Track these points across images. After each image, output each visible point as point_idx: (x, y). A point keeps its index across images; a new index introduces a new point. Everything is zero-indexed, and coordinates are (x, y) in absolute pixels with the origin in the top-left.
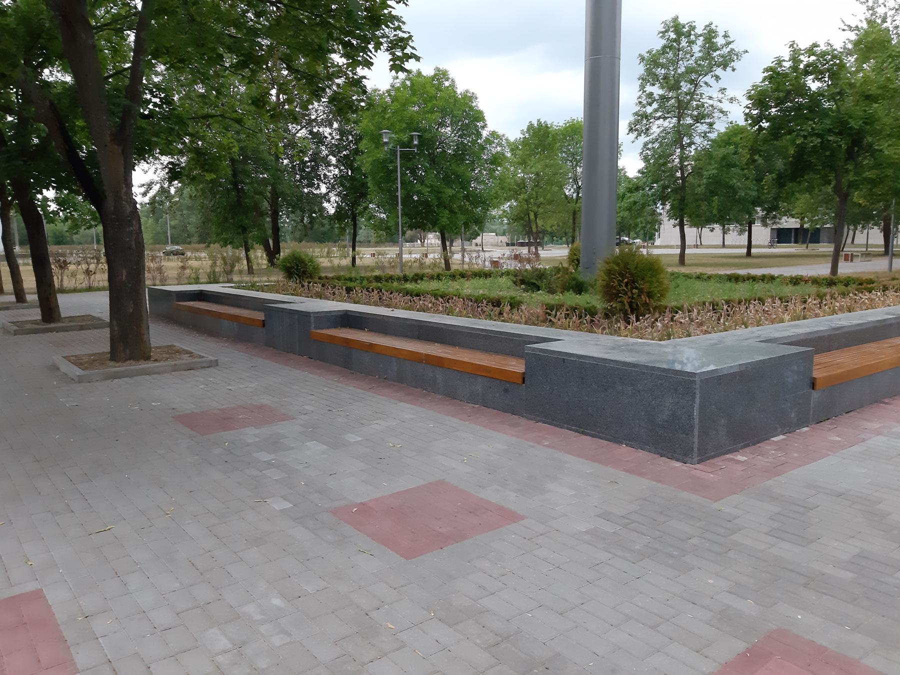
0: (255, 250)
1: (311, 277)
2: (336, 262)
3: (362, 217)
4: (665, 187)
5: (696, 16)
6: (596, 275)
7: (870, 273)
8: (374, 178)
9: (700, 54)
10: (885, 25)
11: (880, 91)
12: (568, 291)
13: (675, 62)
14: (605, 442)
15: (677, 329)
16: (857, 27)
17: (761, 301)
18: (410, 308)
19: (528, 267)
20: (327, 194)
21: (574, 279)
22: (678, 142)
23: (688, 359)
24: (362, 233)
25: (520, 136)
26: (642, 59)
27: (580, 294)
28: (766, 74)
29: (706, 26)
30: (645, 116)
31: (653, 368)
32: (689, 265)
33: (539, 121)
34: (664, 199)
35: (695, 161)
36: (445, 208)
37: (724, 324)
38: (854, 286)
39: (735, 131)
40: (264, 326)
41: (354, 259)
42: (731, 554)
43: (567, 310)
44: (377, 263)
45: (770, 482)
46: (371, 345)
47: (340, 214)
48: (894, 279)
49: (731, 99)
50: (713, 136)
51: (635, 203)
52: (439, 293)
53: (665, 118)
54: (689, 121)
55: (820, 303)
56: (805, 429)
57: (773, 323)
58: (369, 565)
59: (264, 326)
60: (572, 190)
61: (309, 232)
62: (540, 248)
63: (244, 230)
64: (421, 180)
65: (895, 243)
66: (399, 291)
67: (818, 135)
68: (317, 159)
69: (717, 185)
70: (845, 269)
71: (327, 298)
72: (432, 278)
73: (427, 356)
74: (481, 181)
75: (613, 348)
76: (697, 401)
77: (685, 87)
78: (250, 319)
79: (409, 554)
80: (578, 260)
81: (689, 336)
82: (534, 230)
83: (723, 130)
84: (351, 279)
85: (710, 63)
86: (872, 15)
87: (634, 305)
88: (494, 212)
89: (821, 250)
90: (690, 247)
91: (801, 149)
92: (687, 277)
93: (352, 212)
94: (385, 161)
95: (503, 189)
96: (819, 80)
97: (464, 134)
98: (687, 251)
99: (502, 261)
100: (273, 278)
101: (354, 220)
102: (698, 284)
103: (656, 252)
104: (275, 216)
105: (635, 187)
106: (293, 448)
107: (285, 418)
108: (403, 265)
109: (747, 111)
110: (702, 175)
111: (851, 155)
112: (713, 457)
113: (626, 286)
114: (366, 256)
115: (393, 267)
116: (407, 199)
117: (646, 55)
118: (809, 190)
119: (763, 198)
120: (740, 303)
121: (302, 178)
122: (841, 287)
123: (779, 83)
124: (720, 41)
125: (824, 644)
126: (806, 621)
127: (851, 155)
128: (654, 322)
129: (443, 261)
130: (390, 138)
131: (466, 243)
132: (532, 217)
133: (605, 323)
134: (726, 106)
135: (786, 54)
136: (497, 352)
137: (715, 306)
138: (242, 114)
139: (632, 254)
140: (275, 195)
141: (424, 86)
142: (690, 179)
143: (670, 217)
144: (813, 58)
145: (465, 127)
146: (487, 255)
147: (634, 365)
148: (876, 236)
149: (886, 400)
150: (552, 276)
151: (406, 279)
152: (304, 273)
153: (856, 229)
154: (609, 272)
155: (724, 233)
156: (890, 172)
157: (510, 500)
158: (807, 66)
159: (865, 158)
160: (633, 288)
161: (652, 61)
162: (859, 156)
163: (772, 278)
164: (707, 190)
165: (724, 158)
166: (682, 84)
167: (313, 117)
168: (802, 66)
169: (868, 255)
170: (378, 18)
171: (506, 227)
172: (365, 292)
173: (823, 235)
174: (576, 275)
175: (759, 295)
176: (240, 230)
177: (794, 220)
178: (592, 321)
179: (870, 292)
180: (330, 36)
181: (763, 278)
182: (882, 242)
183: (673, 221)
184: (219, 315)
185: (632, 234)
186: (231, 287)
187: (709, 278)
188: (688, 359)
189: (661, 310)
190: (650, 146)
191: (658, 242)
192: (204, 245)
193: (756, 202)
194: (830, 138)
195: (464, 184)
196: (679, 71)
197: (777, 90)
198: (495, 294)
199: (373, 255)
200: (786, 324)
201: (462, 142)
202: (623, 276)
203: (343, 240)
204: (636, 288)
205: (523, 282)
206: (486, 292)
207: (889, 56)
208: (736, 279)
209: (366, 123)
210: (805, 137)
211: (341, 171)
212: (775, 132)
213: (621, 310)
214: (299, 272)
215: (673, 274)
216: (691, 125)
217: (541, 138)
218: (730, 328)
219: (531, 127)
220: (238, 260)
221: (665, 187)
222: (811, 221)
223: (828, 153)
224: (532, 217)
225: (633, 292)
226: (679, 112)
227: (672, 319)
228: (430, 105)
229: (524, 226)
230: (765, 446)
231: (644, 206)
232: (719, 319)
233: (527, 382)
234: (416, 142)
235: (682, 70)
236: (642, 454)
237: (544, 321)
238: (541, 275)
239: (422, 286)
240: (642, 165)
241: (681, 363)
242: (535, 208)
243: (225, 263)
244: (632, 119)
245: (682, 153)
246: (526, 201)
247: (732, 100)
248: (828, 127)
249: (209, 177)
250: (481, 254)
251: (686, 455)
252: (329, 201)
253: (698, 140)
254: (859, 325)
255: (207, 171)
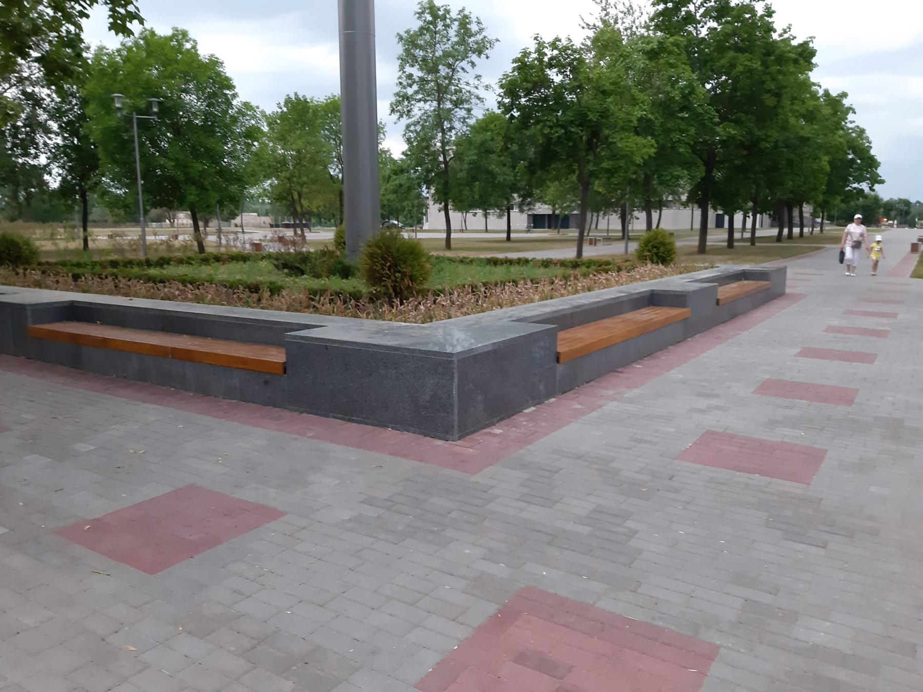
1: (28, 263)
2: (62, 245)
4: (428, 171)
6: (359, 260)
9: (456, 39)
10: (617, 26)
11: (612, 87)
12: (334, 275)
13: (432, 45)
14: (371, 427)
15: (438, 312)
17: (515, 283)
18: (153, 297)
20: (48, 165)
21: (340, 263)
22: (439, 125)
23: (458, 340)
24: (96, 212)
26: (401, 38)
27: (347, 278)
28: (515, 65)
29: (461, 11)
30: (406, 97)
32: (456, 249)
33: (296, 94)
35: (457, 146)
38: (594, 267)
39: (491, 119)
43: (332, 295)
44: (114, 245)
45: (522, 451)
46: (105, 341)
47: (66, 189)
48: (627, 261)
49: (487, 86)
50: (472, 122)
52: (188, 279)
53: (426, 101)
54: (448, 105)
55: (566, 284)
56: (553, 400)
57: (524, 303)
60: (337, 170)
62: (305, 230)
65: (630, 228)
66: (139, 278)
68: (33, 124)
69: (477, 172)
70: (589, 252)
71: (48, 287)
72: (180, 262)
75: (377, 333)
76: (456, 380)
77: (443, 71)
79: (152, 568)
81: (450, 317)
82: (299, 209)
83: (481, 117)
84: (79, 265)
85: (465, 49)
87: (398, 289)
89: (570, 234)
90: (456, 231)
92: (451, 260)
95: (261, 165)
96: (562, 73)
98: (453, 235)
99: (263, 244)
101: (83, 196)
102: (461, 268)
103: (420, 235)
105: (399, 170)
108: (146, 247)
109: (500, 99)
110: (463, 161)
111: (591, 147)
112: (473, 432)
113: (389, 270)
114: (101, 237)
115: (135, 250)
117: (405, 35)
118: (557, 178)
120: (496, 285)
121: (15, 145)
122: (584, 269)
123: (526, 74)
124: (474, 27)
126: (552, 577)
128: (417, 306)
129: (195, 244)
130: (124, 104)
132: (296, 197)
133: (370, 307)
134: (481, 93)
135: (532, 47)
136: (255, 342)
137: (474, 288)
139: (394, 238)
143: (435, 202)
144: (556, 52)
146: (247, 237)
147: (396, 349)
149: (620, 370)
150: (316, 259)
151: (149, 263)
153: (598, 216)
154: (372, 256)
156: (622, 163)
157: (271, 497)
158: (551, 59)
159: (602, 149)
160: (396, 271)
161: (411, 42)
162: (597, 147)
163: (527, 261)
164: (472, 174)
165: (482, 144)
168: (546, 59)
169: (608, 239)
171: (268, 207)
172: (97, 279)
173: (572, 221)
175: (513, 277)
177: (546, 206)
178: (357, 306)
179: (607, 273)
181: (519, 261)
182: (620, 227)
183: (438, 206)
187: (472, 261)
189: (424, 293)
190: (412, 128)
191: (426, 226)
193: (514, 188)
194: (573, 130)
195: (214, 157)
196: (437, 54)
203: (72, 220)
204: (399, 272)
205: (285, 266)
206: (244, 277)
207: (621, 56)
208: (495, 262)
210: (551, 128)
211: (65, 138)
213: (385, 294)
215: (437, 258)
216: (450, 110)
217: (299, 113)
219: (288, 101)
222: (561, 207)
223: (571, 144)
224: (296, 197)
225: (396, 276)
227: (435, 302)
228: (169, 69)
230: (518, 418)
231: (410, 189)
232: (477, 301)
233: (289, 371)
234: (155, 110)
235: (439, 53)
236: (407, 436)
237: (308, 307)
240: (405, 147)
244: (393, 99)
245: (443, 137)
246: (289, 179)
250: (240, 236)
251: (447, 433)
252: (50, 174)
253: (457, 125)
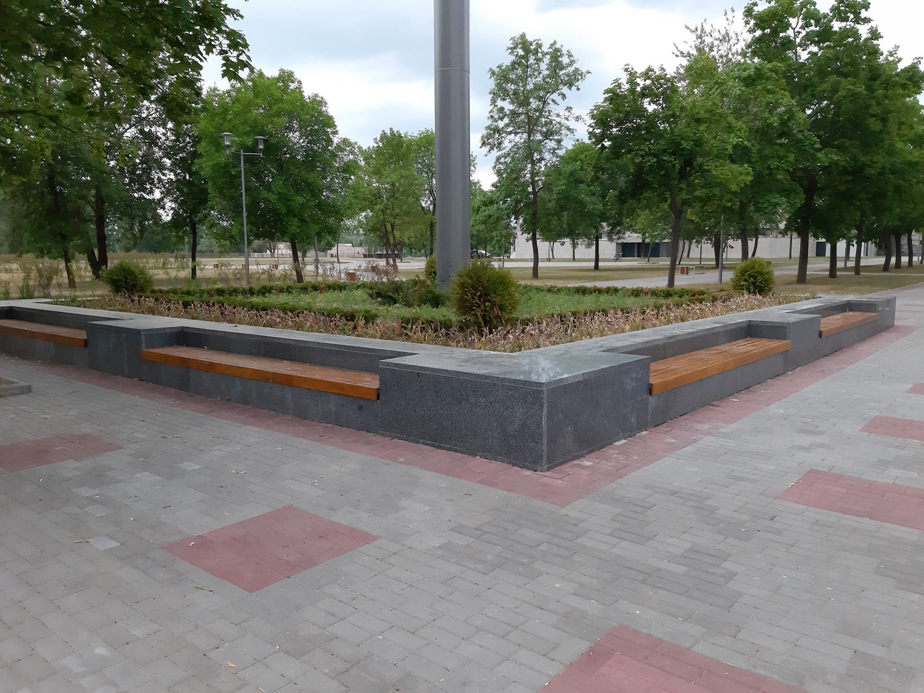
0: (78, 262)
1: (142, 291)
2: (173, 273)
3: (203, 225)
5: (543, 32)
6: (450, 290)
7: (704, 285)
8: (215, 184)
9: (547, 72)
10: (713, 53)
11: (707, 115)
12: (425, 303)
13: (524, 79)
15: (527, 340)
16: (689, 53)
17: (605, 312)
18: (256, 324)
19: (385, 280)
20: (162, 199)
21: (431, 292)
22: (529, 157)
24: (204, 242)
25: (372, 144)
26: (493, 73)
27: (437, 307)
28: (607, 96)
30: (497, 130)
31: (503, 380)
32: (542, 278)
33: (391, 129)
34: (517, 214)
35: (546, 176)
36: (294, 216)
37: (571, 335)
38: (687, 297)
39: (581, 149)
40: (86, 346)
41: (194, 270)
42: (576, 557)
43: (423, 323)
44: (220, 274)
45: (612, 485)
46: (212, 365)
47: (176, 222)
48: (722, 290)
49: (577, 117)
50: (561, 152)
51: (490, 216)
53: (516, 134)
54: (539, 137)
56: (645, 433)
57: (615, 333)
58: (209, 601)
59: (86, 346)
61: (138, 241)
62: (398, 260)
63: (64, 238)
64: (268, 188)
65: (724, 257)
67: (654, 155)
69: (566, 201)
70: (681, 281)
71: (160, 314)
72: (281, 290)
73: (275, 374)
74: (334, 190)
75: (467, 361)
76: (545, 410)
77: (534, 103)
78: (69, 338)
79: (252, 587)
80: (435, 273)
81: (538, 347)
82: (392, 241)
83: (570, 147)
84: (188, 293)
86: (701, 43)
88: (348, 223)
89: (661, 263)
90: (543, 260)
91: (640, 168)
92: (539, 289)
93: (191, 220)
94: (227, 165)
96: (654, 102)
97: (314, 140)
98: (540, 264)
99: (358, 273)
100: (99, 292)
101: (194, 229)
102: (549, 297)
103: (508, 265)
104: (101, 223)
105: (489, 201)
106: (120, 481)
107: (112, 447)
108: (249, 276)
109: (591, 130)
111: (683, 175)
113: (479, 299)
114: (208, 267)
115: (238, 279)
116: (253, 206)
118: (647, 207)
119: (608, 214)
120: (585, 314)
124: (565, 60)
125: (660, 636)
127: (683, 175)
128: (506, 335)
129: (294, 273)
130: (232, 141)
131: (319, 253)
132: (389, 228)
133: (460, 336)
134: (572, 124)
135: (624, 78)
136: (351, 368)
137: (562, 318)
138: (58, 111)
139: (485, 268)
140: (100, 200)
141: (268, 88)
142: (540, 194)
144: (648, 82)
145: (313, 133)
146: (343, 266)
148: (708, 251)
149: (715, 403)
151: (251, 292)
152: (134, 286)
154: (463, 286)
155: (574, 247)
157: (362, 520)
159: (696, 178)
160: (485, 301)
161: (502, 77)
163: (616, 290)
164: (557, 204)
165: (572, 174)
166: (531, 100)
167: (144, 115)
168: (638, 89)
169: (701, 268)
170: (212, 17)
171: (362, 238)
173: (663, 249)
174: (432, 288)
175: (603, 307)
176: (59, 239)
177: (636, 235)
180: (156, 32)
181: (608, 290)
183: (526, 235)
184: (33, 335)
185: (489, 247)
186: (48, 303)
187: (559, 290)
188: (543, 369)
189: (513, 322)
190: (502, 160)
191: (513, 256)
192: (13, 256)
193: (603, 217)
194: (665, 158)
195: (314, 192)
196: (528, 88)
197: (617, 111)
198: (349, 307)
199: (216, 266)
200: (627, 333)
201: (312, 149)
202: (476, 289)
203: (181, 250)
204: (489, 301)
205: (379, 295)
206: (341, 306)
207: (716, 83)
208: (583, 291)
209: (204, 124)
210: (643, 156)
211: (176, 175)
212: (616, 152)
213: (474, 323)
214: (128, 285)
215: (525, 287)
216: (540, 141)
217: (394, 148)
218: (576, 338)
219: (384, 136)
220: (56, 271)
221: (518, 202)
222: (651, 236)
223: (663, 173)
224: (389, 228)
225: (485, 306)
226: (529, 128)
227: (523, 331)
229: (381, 238)
230: (609, 451)
231: (498, 219)
232: (566, 331)
233: (382, 398)
234: (261, 147)
235: (530, 86)
236: (496, 465)
237: (400, 335)
238: (398, 288)
239: (271, 299)
240: (495, 179)
241: (538, 374)
242: (391, 219)
243: (41, 276)
244: (485, 132)
246: (382, 211)
247: (578, 118)
248: (663, 147)
249: (16, 180)
250: (336, 265)
252: (164, 208)
253: (547, 156)
254: (689, 333)
255: (15, 173)
